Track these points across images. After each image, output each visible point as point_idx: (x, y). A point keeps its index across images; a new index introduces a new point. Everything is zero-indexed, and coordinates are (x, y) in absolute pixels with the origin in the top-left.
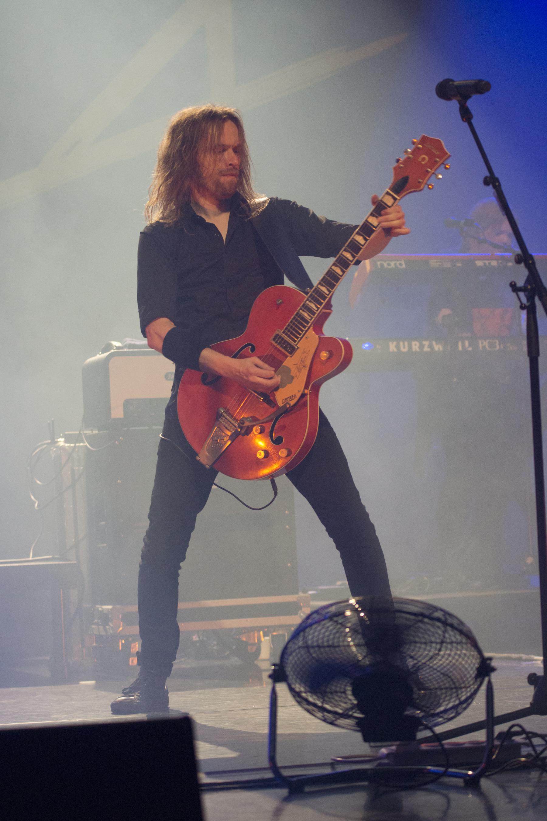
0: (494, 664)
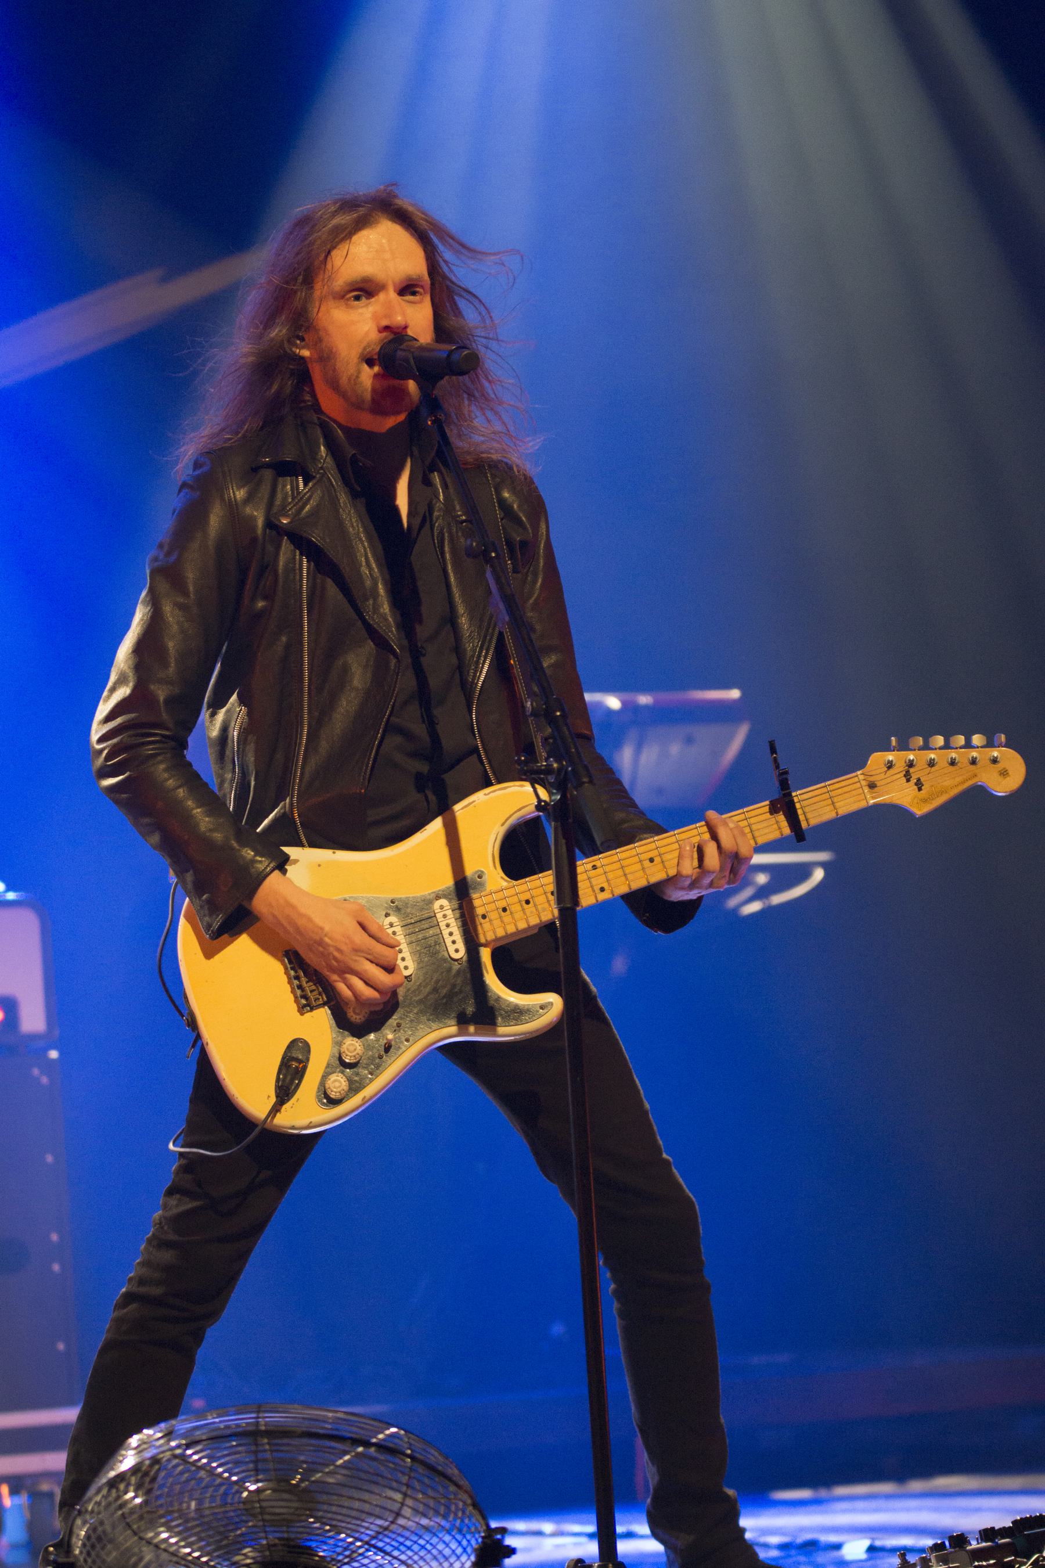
0: (510, 1541)
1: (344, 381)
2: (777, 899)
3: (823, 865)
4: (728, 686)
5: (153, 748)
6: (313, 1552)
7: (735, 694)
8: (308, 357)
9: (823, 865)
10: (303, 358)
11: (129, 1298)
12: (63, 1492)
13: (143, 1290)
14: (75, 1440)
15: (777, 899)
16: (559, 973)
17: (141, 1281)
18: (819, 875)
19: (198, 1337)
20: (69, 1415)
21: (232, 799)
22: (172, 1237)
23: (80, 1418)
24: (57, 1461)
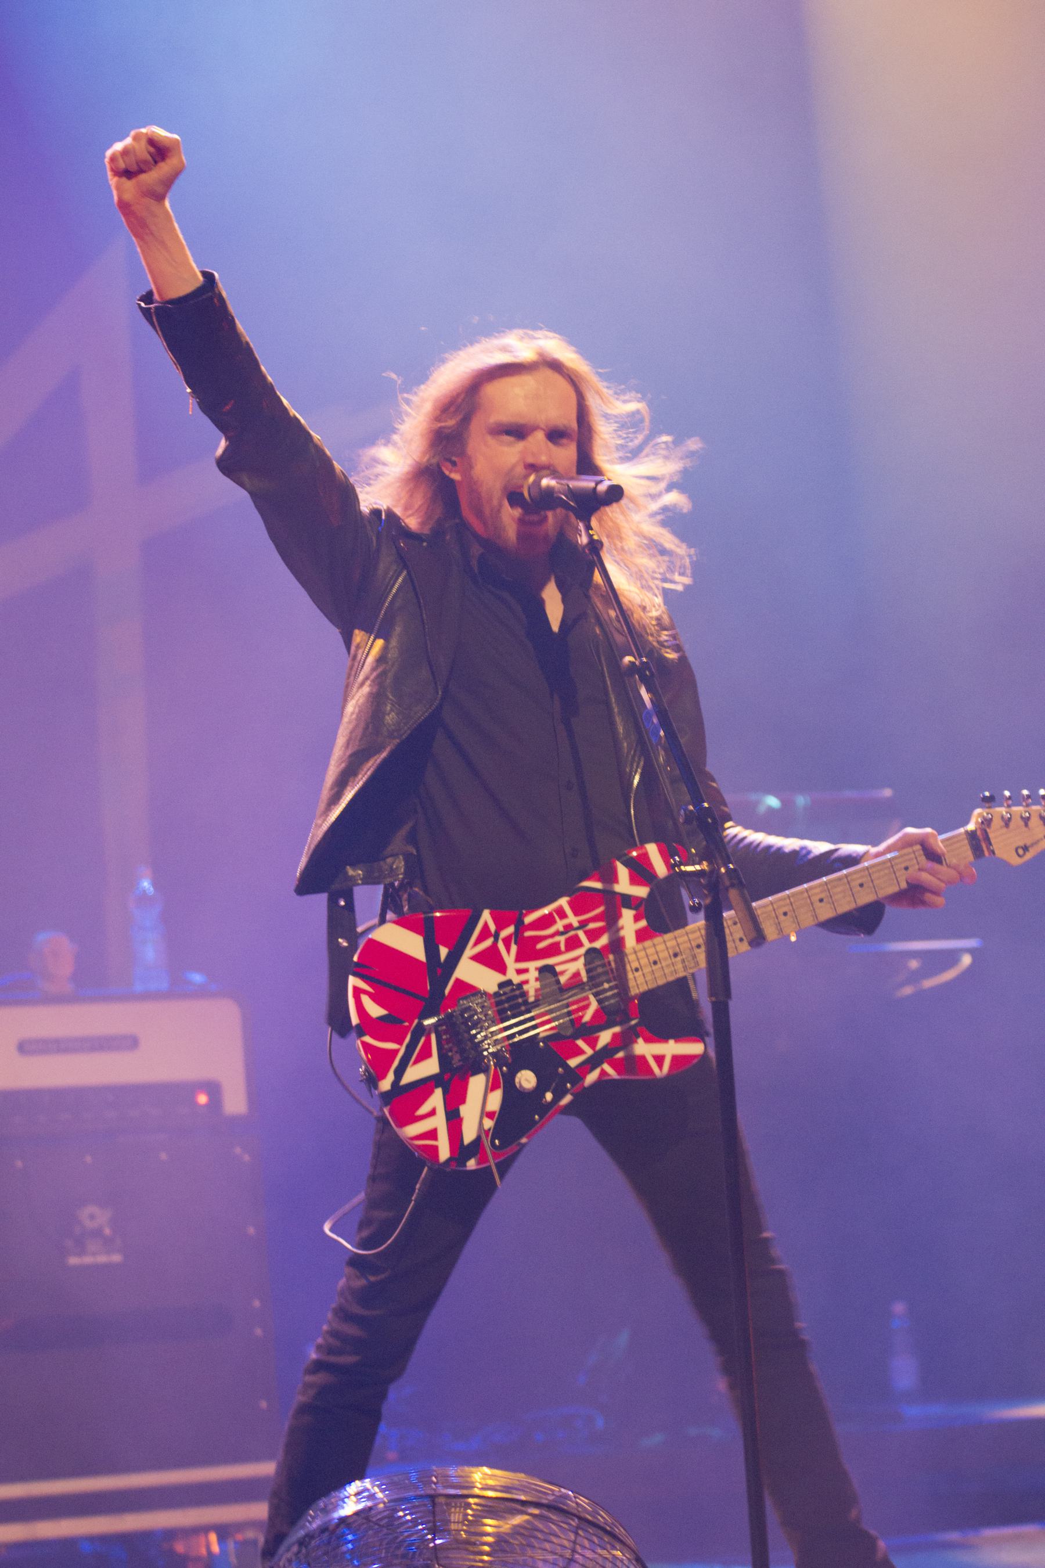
1: (487, 512)
2: (929, 983)
3: (971, 951)
4: (359, 958)
5: (564, 1505)
6: (472, 1485)
7: (355, 959)
8: (458, 481)
9: (971, 951)
10: (452, 481)
11: (318, 1366)
12: (266, 1542)
13: (333, 1359)
14: (275, 1494)
15: (929, 983)
16: (570, 1020)
17: (330, 1350)
18: (967, 960)
19: (383, 1396)
20: (267, 1468)
21: (594, 654)
22: (357, 1310)
23: (278, 1473)
24: (260, 1511)
